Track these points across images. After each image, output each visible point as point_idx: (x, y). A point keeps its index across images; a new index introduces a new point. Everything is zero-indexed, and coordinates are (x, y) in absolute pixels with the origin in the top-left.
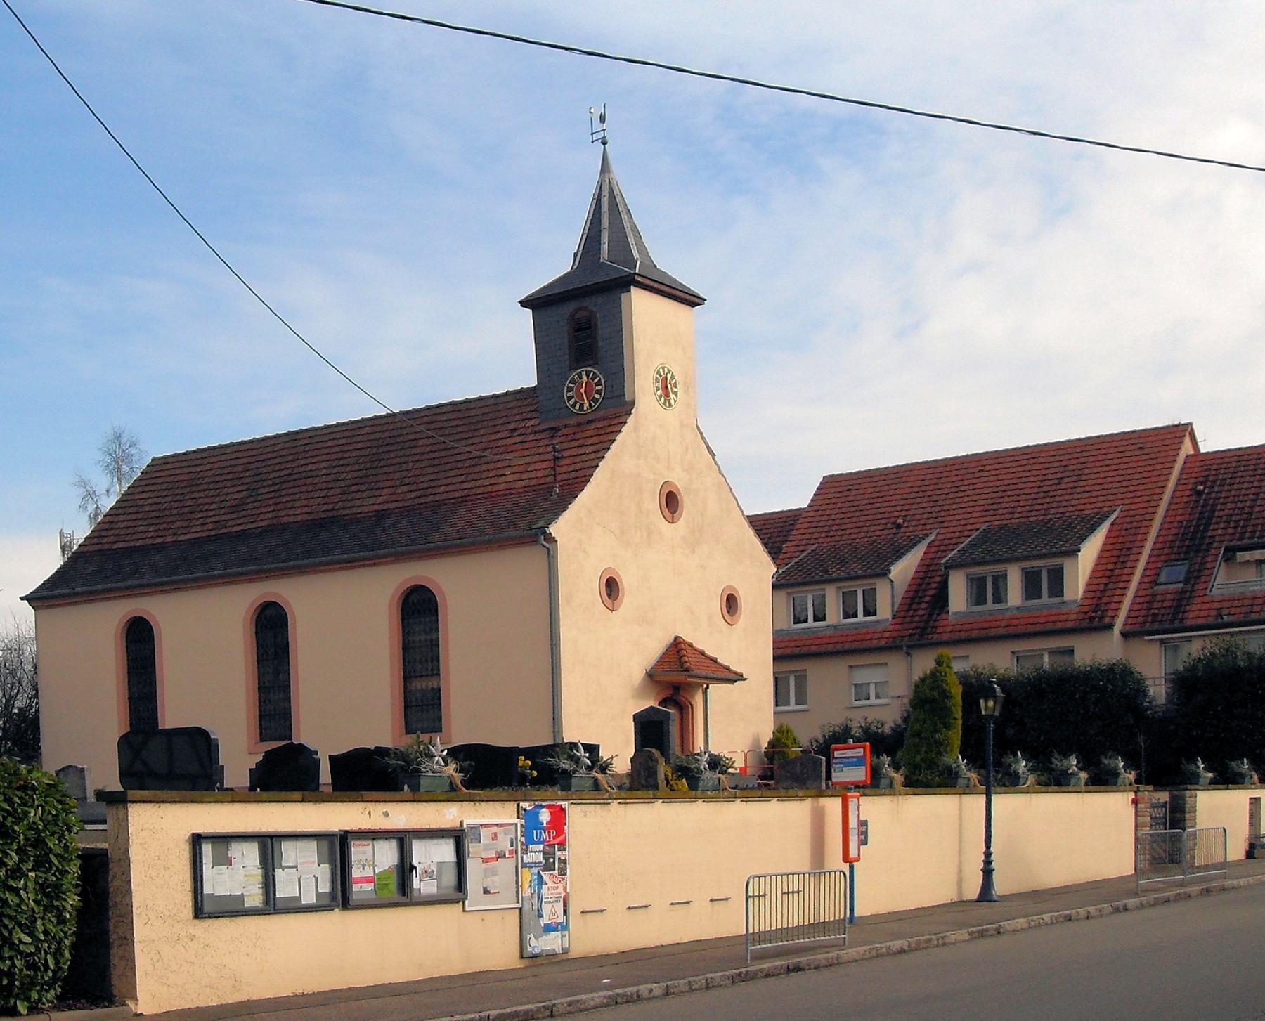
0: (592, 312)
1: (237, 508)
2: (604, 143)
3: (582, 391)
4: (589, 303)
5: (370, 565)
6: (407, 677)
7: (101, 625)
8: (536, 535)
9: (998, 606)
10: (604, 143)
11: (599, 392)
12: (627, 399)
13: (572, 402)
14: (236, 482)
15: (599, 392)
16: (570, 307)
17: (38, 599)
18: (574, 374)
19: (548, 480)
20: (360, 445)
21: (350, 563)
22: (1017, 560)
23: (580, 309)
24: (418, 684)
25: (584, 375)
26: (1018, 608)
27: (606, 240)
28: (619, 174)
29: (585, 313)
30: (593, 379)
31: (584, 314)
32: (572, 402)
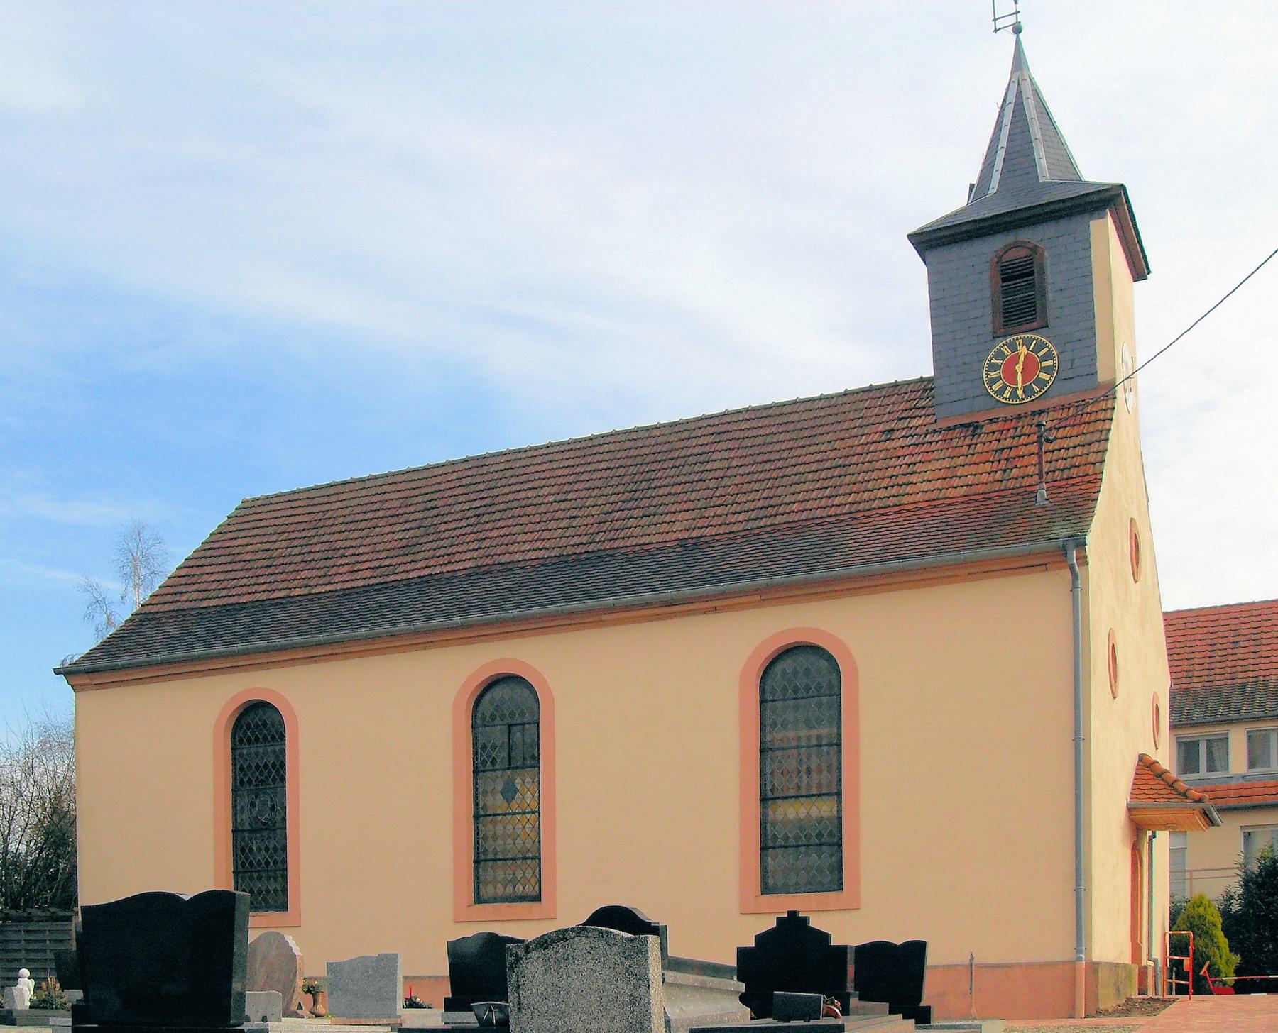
0: (1034, 250)
1: (407, 548)
2: (1017, 30)
3: (1019, 368)
4: (1029, 235)
5: (705, 612)
6: (766, 798)
7: (189, 719)
8: (1064, 551)
9: (1213, 775)
10: (1017, 30)
11: (1048, 370)
12: (1102, 377)
13: (996, 387)
14: (394, 520)
15: (1048, 370)
16: (998, 243)
17: (80, 674)
18: (1002, 345)
19: (1027, 481)
20: (602, 466)
21: (670, 608)
22: (1238, 721)
23: (1015, 246)
24: (789, 812)
25: (1022, 345)
26: (1244, 777)
27: (1043, 154)
28: (1038, 70)
29: (1022, 253)
30: (1036, 350)
31: (1026, 248)
32: (996, 387)
